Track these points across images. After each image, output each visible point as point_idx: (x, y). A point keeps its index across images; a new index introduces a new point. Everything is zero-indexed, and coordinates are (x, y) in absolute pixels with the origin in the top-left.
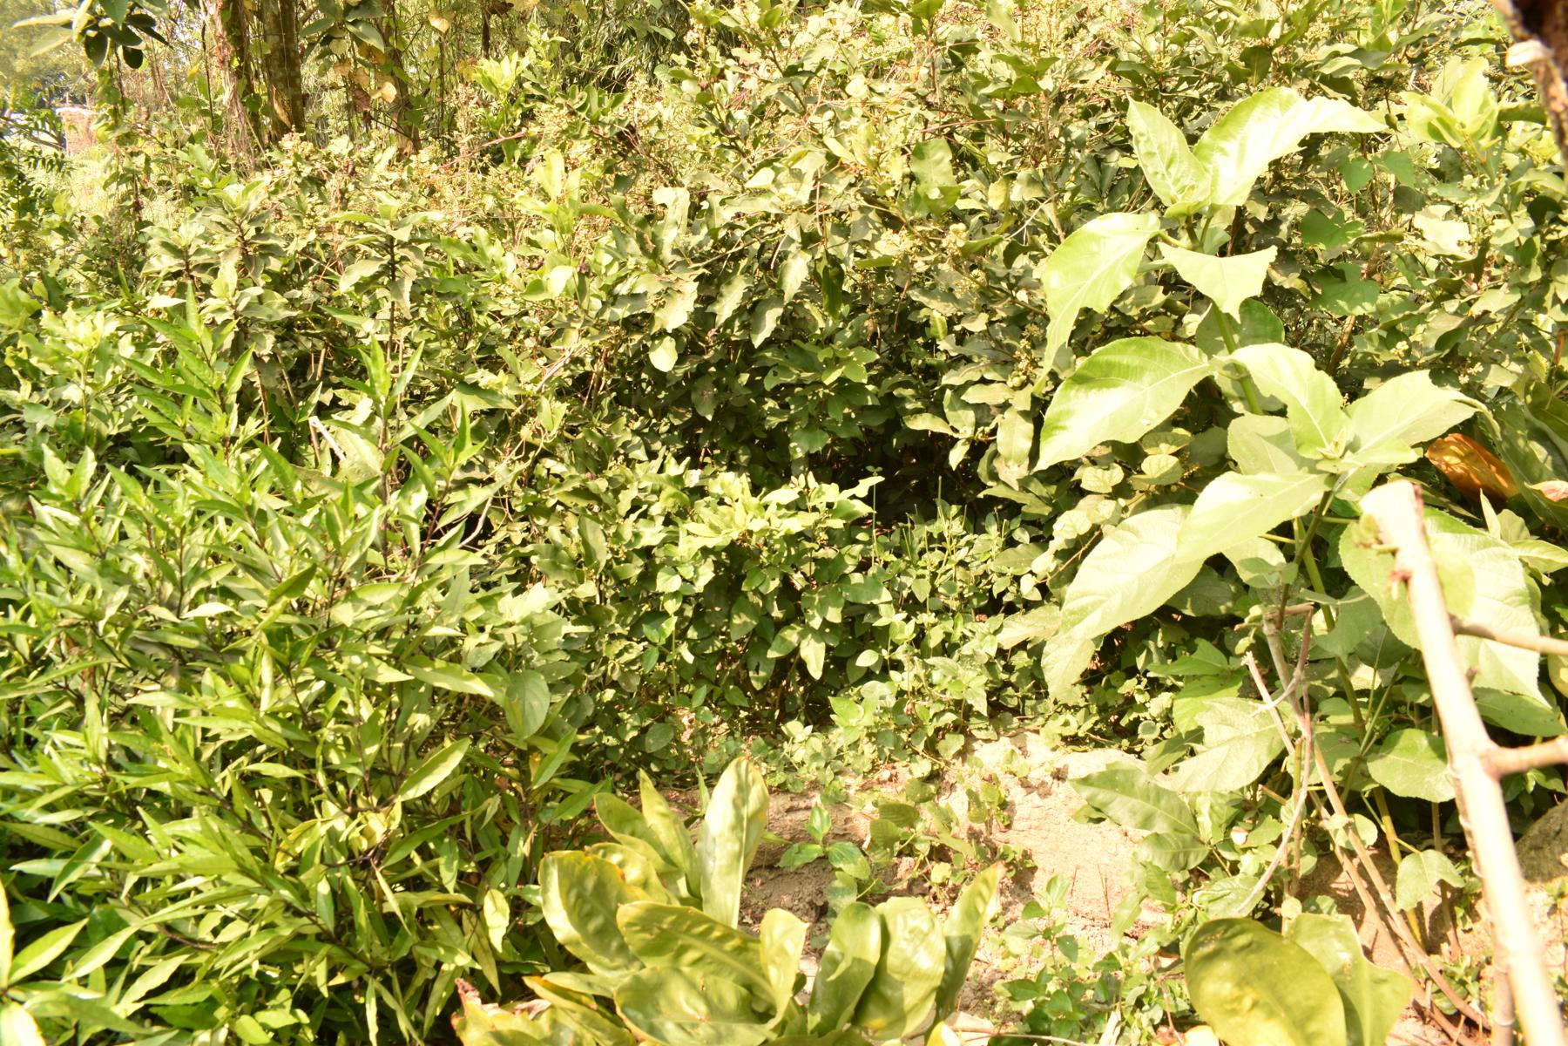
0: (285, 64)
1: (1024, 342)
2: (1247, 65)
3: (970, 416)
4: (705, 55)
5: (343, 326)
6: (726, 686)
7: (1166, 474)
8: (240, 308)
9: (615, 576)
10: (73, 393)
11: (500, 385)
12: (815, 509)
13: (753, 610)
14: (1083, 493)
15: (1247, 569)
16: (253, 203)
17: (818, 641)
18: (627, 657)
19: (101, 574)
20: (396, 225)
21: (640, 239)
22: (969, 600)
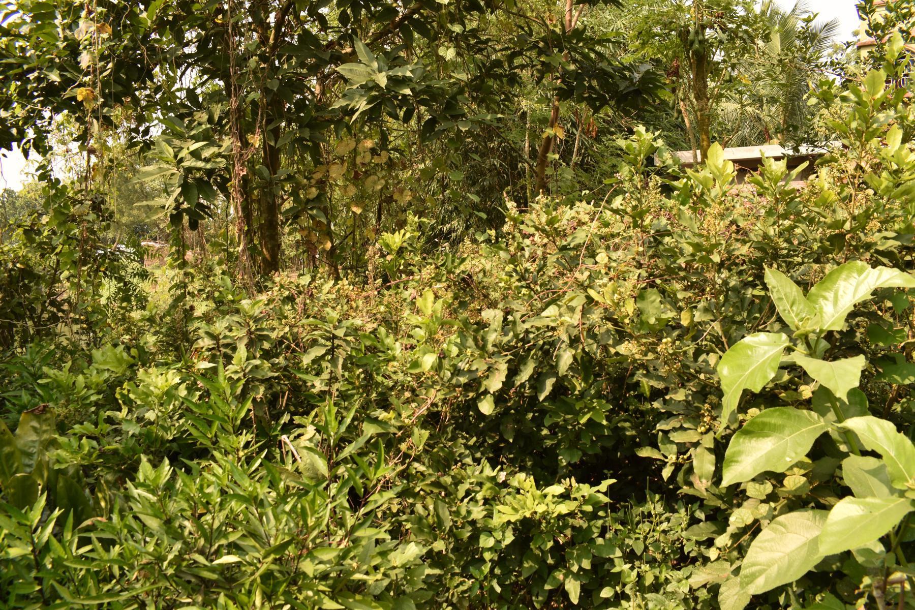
0: (271, 233)
1: (707, 406)
2: (831, 245)
3: (674, 448)
4: (514, 238)
5: (300, 379)
6: (517, 605)
7: (799, 488)
8: (247, 370)
9: (455, 536)
10: (151, 415)
11: (390, 419)
12: (575, 499)
13: (535, 558)
14: (748, 498)
15: (862, 555)
16: (256, 312)
17: (576, 580)
18: (461, 588)
19: (167, 533)
20: (335, 328)
21: (475, 340)
22: (668, 555)
